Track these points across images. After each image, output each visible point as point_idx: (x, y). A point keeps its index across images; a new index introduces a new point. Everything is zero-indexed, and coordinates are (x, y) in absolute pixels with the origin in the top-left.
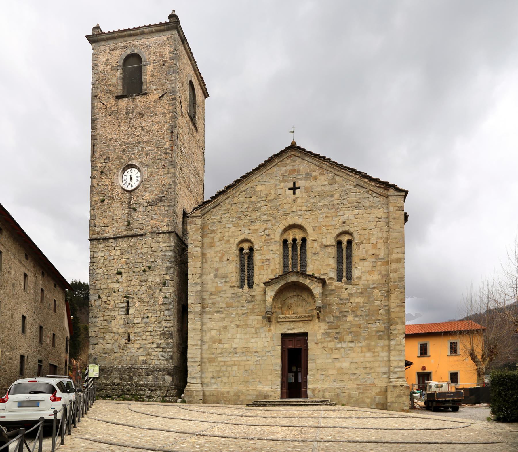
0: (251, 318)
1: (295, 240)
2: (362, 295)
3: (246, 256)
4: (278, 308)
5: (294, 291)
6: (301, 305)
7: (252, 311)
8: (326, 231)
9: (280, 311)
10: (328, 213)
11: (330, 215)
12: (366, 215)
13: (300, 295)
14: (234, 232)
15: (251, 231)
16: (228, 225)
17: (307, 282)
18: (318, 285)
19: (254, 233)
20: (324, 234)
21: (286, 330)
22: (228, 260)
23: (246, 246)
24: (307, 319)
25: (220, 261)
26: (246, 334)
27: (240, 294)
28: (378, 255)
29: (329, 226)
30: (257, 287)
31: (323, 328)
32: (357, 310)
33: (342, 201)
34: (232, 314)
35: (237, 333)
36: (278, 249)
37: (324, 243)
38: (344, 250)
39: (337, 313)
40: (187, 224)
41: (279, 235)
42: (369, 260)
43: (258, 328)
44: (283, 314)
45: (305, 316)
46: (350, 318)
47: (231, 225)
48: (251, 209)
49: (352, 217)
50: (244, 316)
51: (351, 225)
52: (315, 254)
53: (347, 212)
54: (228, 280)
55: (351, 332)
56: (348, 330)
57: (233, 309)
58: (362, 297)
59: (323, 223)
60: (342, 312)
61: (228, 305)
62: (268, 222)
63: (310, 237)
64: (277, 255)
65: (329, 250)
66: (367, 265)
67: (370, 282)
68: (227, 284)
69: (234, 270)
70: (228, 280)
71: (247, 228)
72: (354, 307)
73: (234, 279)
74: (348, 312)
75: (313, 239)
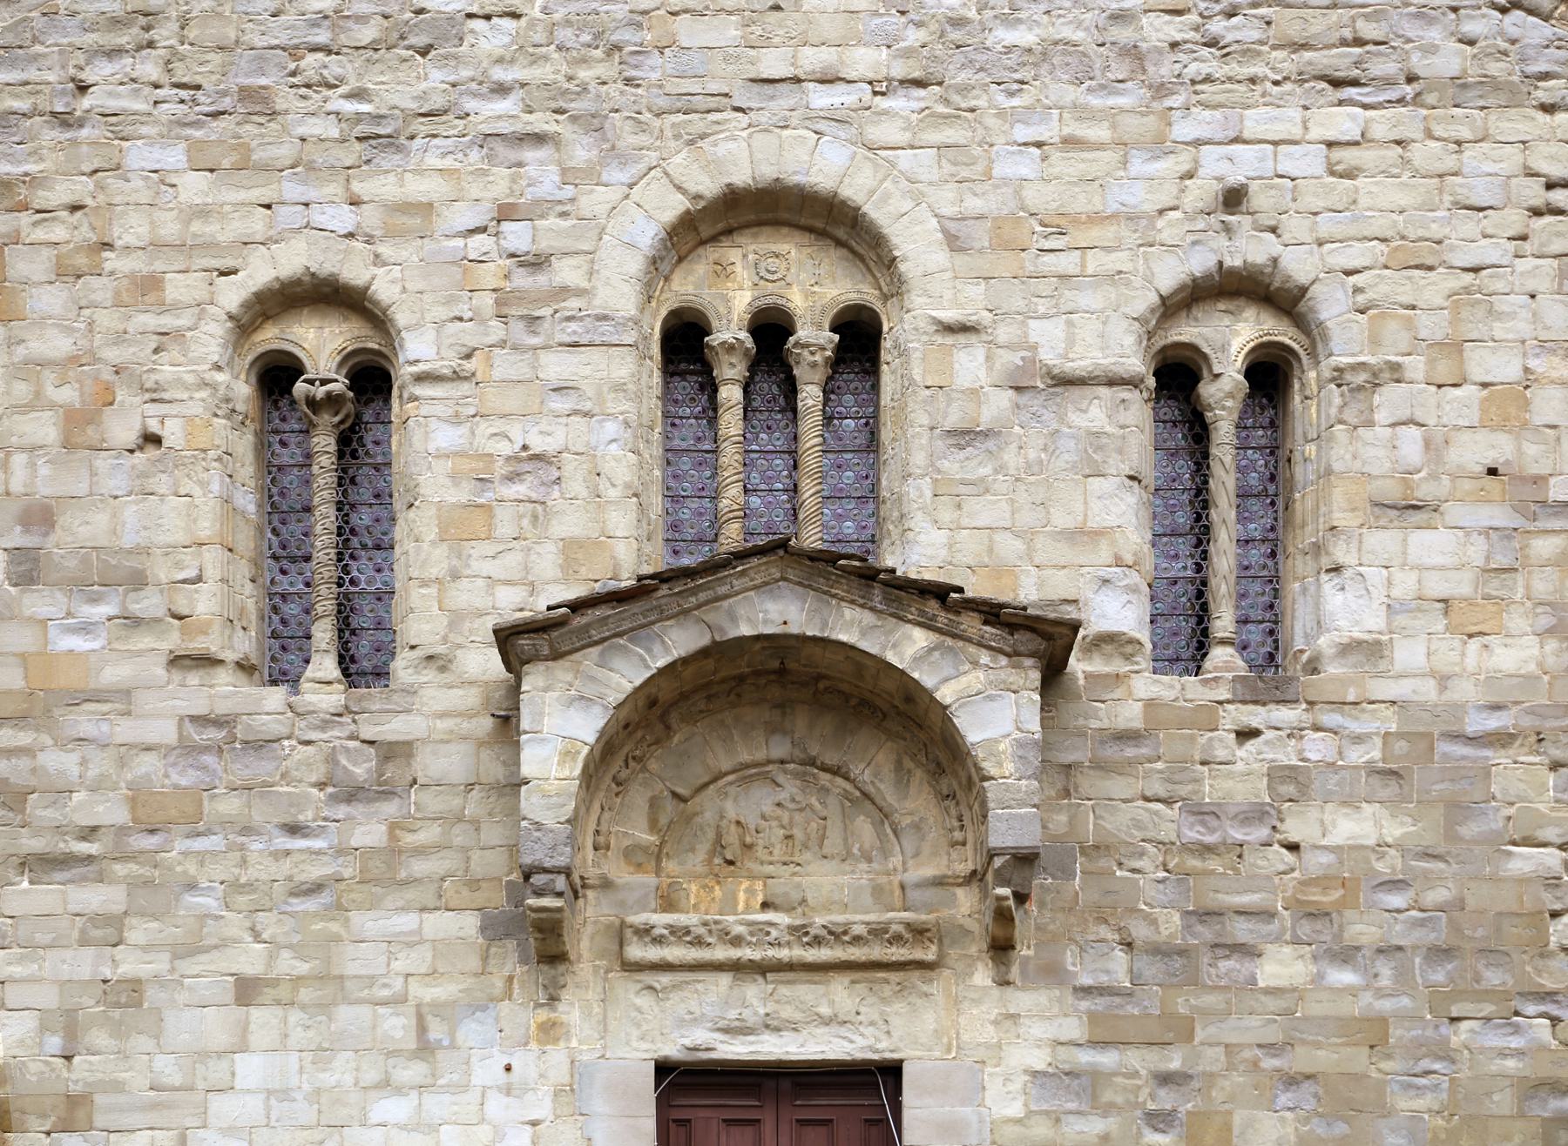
0: (367, 922)
1: (771, 330)
2: (1392, 789)
3: (325, 410)
5: (773, 729)
6: (834, 842)
7: (383, 873)
8: (1067, 263)
9: (650, 880)
10: (1082, 112)
11: (1100, 132)
12: (1426, 154)
13: (831, 758)
14: (203, 212)
15: (370, 218)
16: (139, 156)
17: (910, 651)
18: (1014, 677)
19: (392, 233)
20: (1044, 287)
22: (153, 439)
23: (321, 344)
24: (897, 953)
25: (68, 445)
26: (322, 1053)
27: (270, 725)
28: (1539, 480)
29: (1096, 219)
30: (429, 675)
31: (1039, 1030)
32: (1342, 904)
33: (1217, 26)
34: (192, 886)
35: (243, 1048)
36: (630, 375)
37: (1049, 356)
38: (1226, 402)
39: (1171, 924)
41: (635, 264)
42: (1455, 512)
43: (441, 1009)
44: (668, 905)
45: (878, 932)
46: (1281, 967)
47: (174, 157)
48: (367, 34)
49: (1306, 162)
50: (311, 904)
51: (1295, 226)
52: (964, 436)
53: (1256, 121)
54: (148, 603)
55: (1291, 1081)
56: (1269, 1063)
57: (199, 844)
58: (1393, 805)
59: (1036, 197)
60: (1207, 915)
61: (152, 816)
62: (531, 154)
63: (916, 300)
64: (611, 428)
65: (1094, 413)
66: (1439, 553)
67: (1464, 691)
68: (144, 641)
69: (206, 527)
70: (148, 603)
71: (334, 189)
72: (1323, 881)
73: (204, 603)
74: (1268, 915)
75: (949, 315)
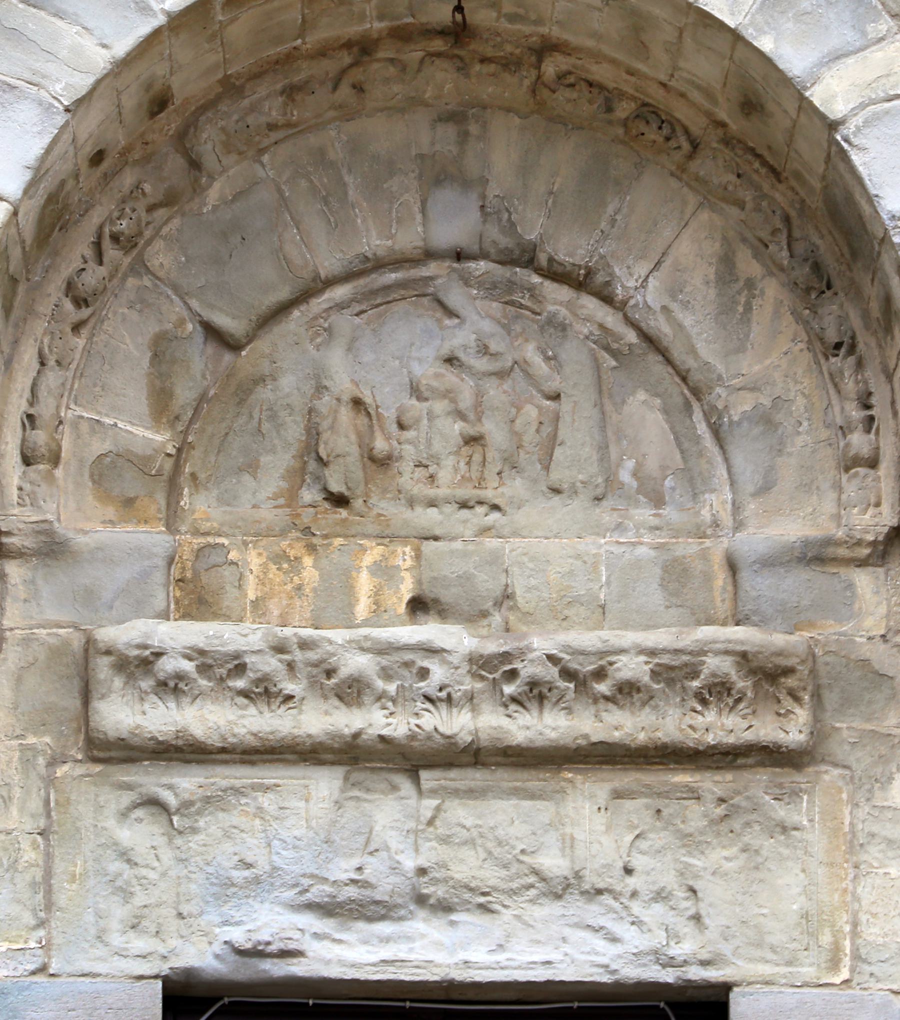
4: (104, 473)
9: (153, 538)
13: (571, 248)
21: (267, 921)
24: (720, 726)
40: (126, 949)
44: (196, 598)
45: (675, 674)
